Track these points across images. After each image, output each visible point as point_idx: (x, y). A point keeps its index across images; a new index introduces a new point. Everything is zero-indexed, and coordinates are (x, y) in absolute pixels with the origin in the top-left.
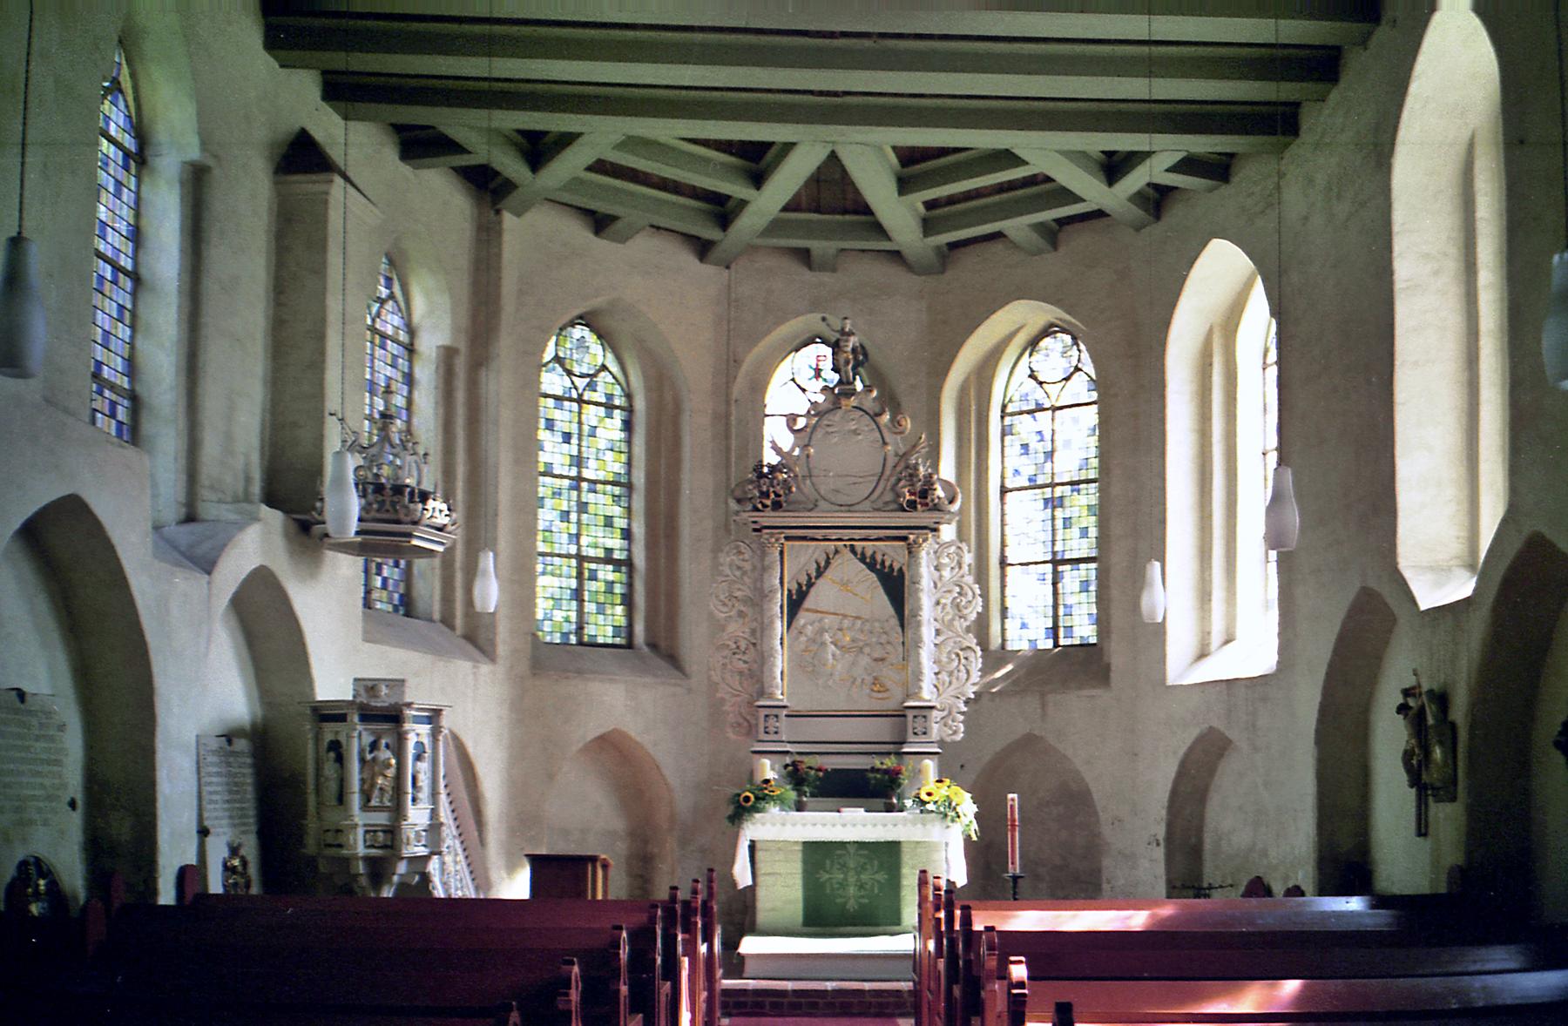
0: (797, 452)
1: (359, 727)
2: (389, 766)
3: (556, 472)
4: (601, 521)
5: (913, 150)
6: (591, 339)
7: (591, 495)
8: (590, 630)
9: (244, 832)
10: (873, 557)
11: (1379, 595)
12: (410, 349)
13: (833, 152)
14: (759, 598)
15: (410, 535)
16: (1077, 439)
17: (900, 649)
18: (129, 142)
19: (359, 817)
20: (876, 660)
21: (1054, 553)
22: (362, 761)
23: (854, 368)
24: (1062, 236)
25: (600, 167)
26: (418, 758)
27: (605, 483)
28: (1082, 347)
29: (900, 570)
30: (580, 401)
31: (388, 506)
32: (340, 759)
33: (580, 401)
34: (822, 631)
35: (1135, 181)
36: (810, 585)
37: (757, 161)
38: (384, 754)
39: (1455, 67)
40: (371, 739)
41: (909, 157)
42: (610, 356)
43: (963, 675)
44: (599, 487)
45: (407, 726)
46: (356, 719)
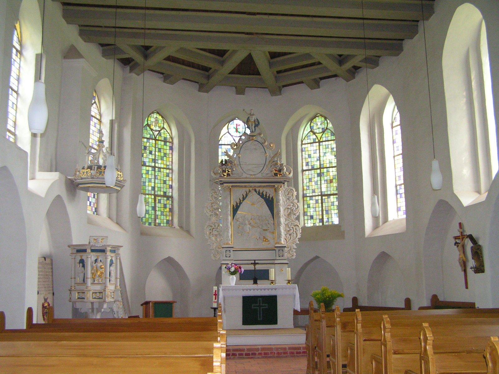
5: (275, 53)
9: (49, 293)
12: (100, 121)
13: (250, 53)
17: (273, 226)
21: (321, 192)
23: (255, 127)
24: (283, 89)
25: (170, 59)
26: (111, 265)
27: (164, 168)
28: (328, 121)
29: (272, 198)
33: (156, 140)
35: (349, 65)
36: (240, 203)
41: (273, 55)
43: (295, 235)
44: (162, 170)
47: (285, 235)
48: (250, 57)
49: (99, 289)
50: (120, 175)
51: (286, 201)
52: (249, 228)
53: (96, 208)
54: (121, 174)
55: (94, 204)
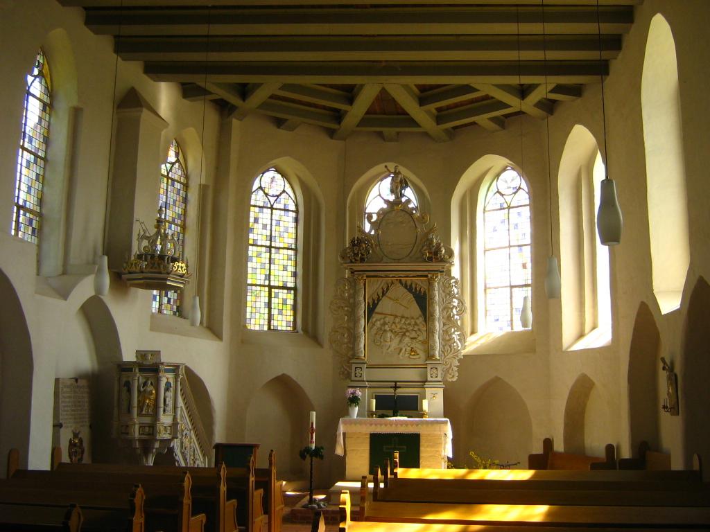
0: (373, 233)
1: (138, 375)
2: (152, 394)
3: (259, 243)
4: (281, 268)
6: (278, 176)
7: (277, 255)
8: (274, 323)
10: (411, 286)
11: (647, 305)
14: (354, 307)
15: (166, 279)
16: (522, 224)
18: (46, 99)
19: (136, 419)
20: (412, 338)
22: (139, 391)
26: (167, 389)
29: (425, 293)
30: (272, 208)
31: (156, 265)
32: (129, 391)
33: (272, 208)
34: (385, 324)
35: (534, 97)
36: (379, 300)
37: (350, 94)
38: (150, 388)
39: (660, 48)
40: (144, 380)
41: (423, 88)
42: (287, 185)
45: (161, 374)
46: (137, 371)
47: (443, 346)
48: (384, 92)
49: (149, 422)
50: (182, 267)
51: (446, 297)
52: (391, 337)
53: (178, 307)
54: (183, 265)
55: (175, 301)
